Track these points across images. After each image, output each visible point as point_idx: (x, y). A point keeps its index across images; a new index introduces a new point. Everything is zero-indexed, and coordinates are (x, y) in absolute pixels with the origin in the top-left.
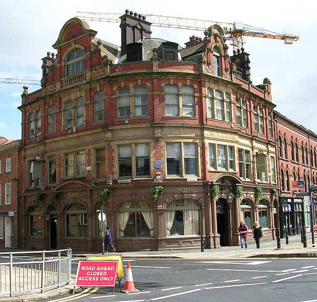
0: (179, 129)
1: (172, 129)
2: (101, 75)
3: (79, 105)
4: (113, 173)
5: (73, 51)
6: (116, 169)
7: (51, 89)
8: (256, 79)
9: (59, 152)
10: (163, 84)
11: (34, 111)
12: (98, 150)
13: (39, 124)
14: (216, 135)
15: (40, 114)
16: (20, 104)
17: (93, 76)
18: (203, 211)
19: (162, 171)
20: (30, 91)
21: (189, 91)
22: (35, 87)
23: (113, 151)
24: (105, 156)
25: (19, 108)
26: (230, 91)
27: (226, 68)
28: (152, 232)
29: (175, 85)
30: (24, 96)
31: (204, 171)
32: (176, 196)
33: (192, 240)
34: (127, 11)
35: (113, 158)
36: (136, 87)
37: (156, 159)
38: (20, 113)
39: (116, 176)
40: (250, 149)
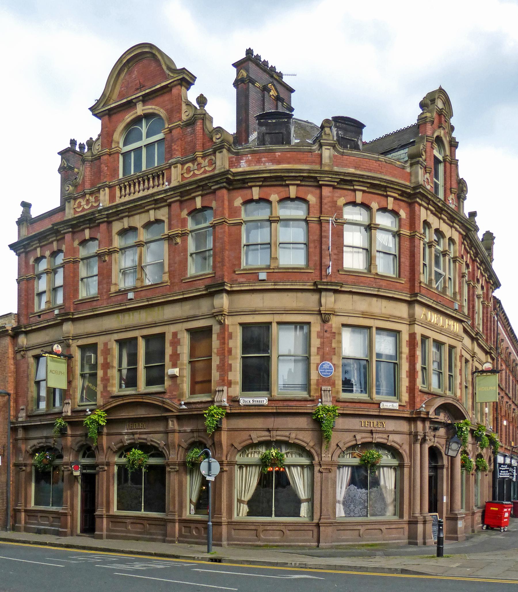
0: (368, 299)
1: (356, 297)
2: (205, 172)
3: (326, 191)
4: (230, 384)
5: (138, 120)
6: (236, 375)
7: (87, 204)
8: (468, 208)
9: (173, 328)
10: (341, 201)
11: (47, 253)
12: (193, 332)
13: (59, 280)
14: (434, 318)
15: (60, 259)
16: (15, 239)
17: (186, 175)
18: (406, 470)
19: (333, 384)
20: (35, 213)
21: (298, 211)
22: (47, 197)
23: (230, 336)
24: (332, 328)
25: (12, 247)
26: (456, 236)
27: (388, 189)
28: (304, 508)
29: (264, 200)
30: (25, 221)
31: (412, 389)
32: (358, 437)
33: (383, 527)
34: (73, 142)
35: (230, 351)
36: (285, 199)
37: (323, 358)
38: (13, 258)
39: (236, 390)
40: (469, 357)
